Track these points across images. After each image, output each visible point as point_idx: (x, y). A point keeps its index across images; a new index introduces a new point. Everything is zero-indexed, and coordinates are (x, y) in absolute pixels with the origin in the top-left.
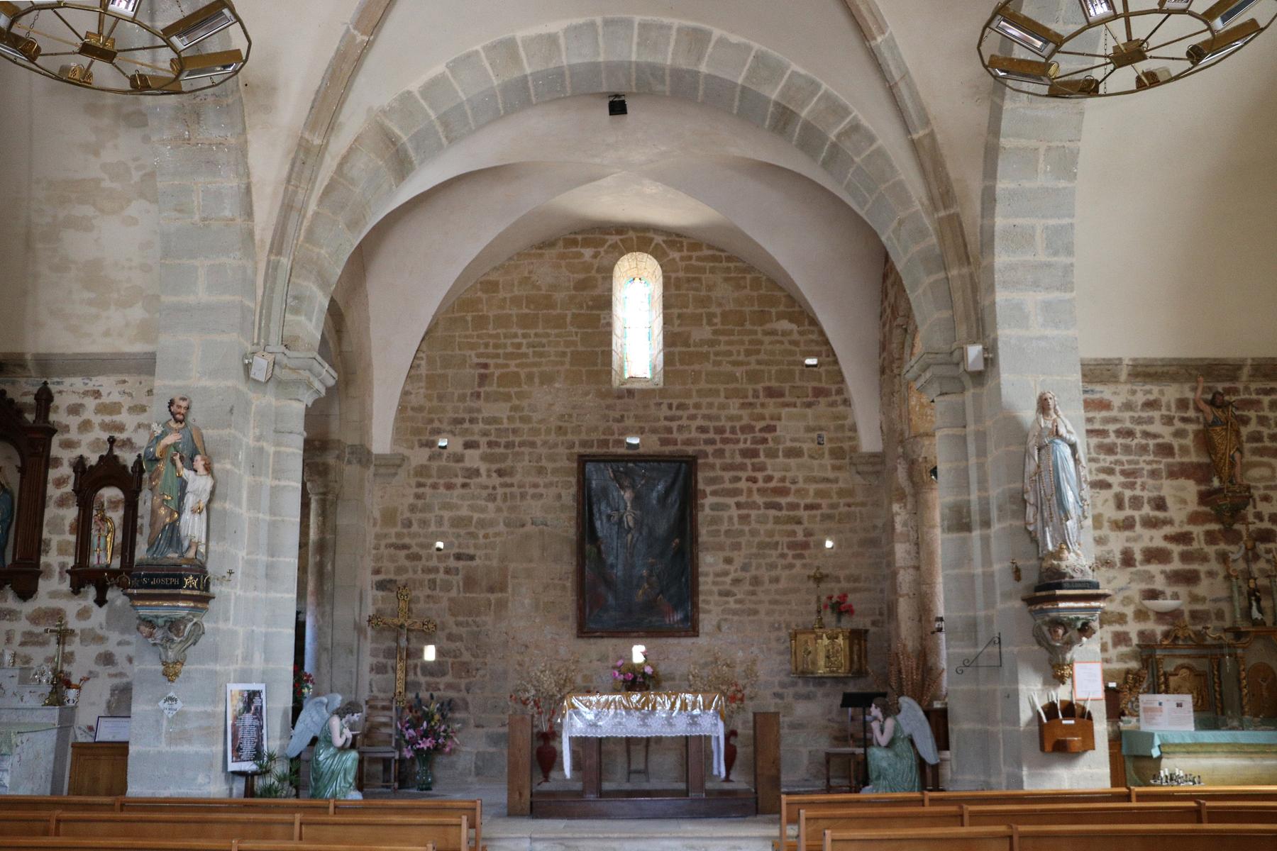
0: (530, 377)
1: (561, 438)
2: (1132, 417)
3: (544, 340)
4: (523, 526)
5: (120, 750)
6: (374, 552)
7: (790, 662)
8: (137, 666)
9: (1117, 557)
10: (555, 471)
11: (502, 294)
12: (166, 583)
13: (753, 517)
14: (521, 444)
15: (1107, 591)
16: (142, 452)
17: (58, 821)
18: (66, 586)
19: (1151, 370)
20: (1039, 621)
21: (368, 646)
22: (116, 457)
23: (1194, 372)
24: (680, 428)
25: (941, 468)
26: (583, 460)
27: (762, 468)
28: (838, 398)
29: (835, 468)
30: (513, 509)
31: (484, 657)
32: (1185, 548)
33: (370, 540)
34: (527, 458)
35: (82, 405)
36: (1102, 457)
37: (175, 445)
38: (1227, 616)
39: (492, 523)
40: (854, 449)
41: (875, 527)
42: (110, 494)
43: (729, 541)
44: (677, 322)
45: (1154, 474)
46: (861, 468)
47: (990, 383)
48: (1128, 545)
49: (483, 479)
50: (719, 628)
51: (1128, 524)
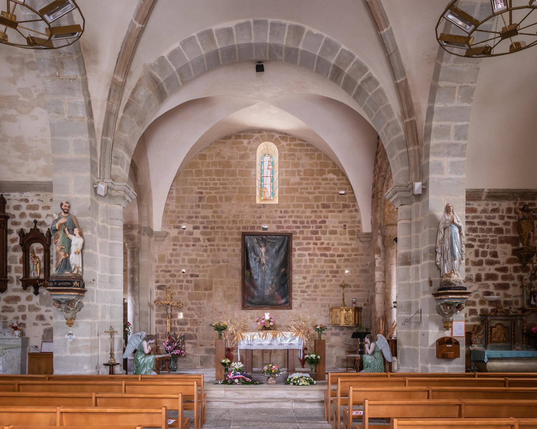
0: (221, 198)
1: (235, 225)
2: (486, 216)
3: (227, 182)
4: (219, 263)
5: (50, 355)
6: (156, 273)
7: (329, 320)
8: (54, 320)
9: (474, 277)
10: (232, 239)
11: (208, 160)
12: (70, 287)
13: (315, 260)
14: (218, 228)
15: (470, 291)
16: (50, 227)
17: (19, 385)
18: (20, 287)
19: (497, 194)
20: (439, 304)
21: (154, 313)
22: (38, 229)
23: (516, 196)
24: (285, 221)
25: (400, 237)
26: (244, 235)
27: (319, 239)
28: (353, 209)
29: (351, 239)
30: (214, 255)
31: (203, 317)
32: (504, 274)
33: (154, 269)
34: (220, 234)
35: (20, 206)
36: (471, 233)
37: (65, 224)
38: (520, 303)
39: (205, 261)
40: (359, 231)
41: (367, 265)
42: (36, 246)
43: (305, 270)
44: (284, 174)
45: (493, 241)
46: (362, 239)
47: (424, 200)
48: (479, 272)
49: (202, 243)
50: (300, 306)
51: (480, 263)
